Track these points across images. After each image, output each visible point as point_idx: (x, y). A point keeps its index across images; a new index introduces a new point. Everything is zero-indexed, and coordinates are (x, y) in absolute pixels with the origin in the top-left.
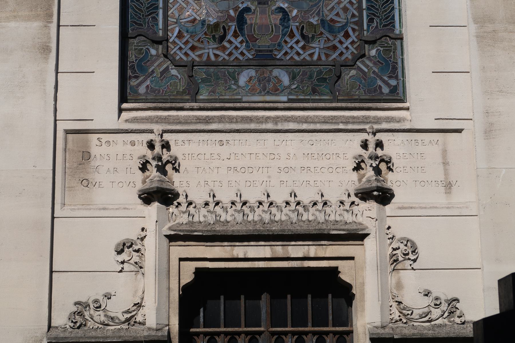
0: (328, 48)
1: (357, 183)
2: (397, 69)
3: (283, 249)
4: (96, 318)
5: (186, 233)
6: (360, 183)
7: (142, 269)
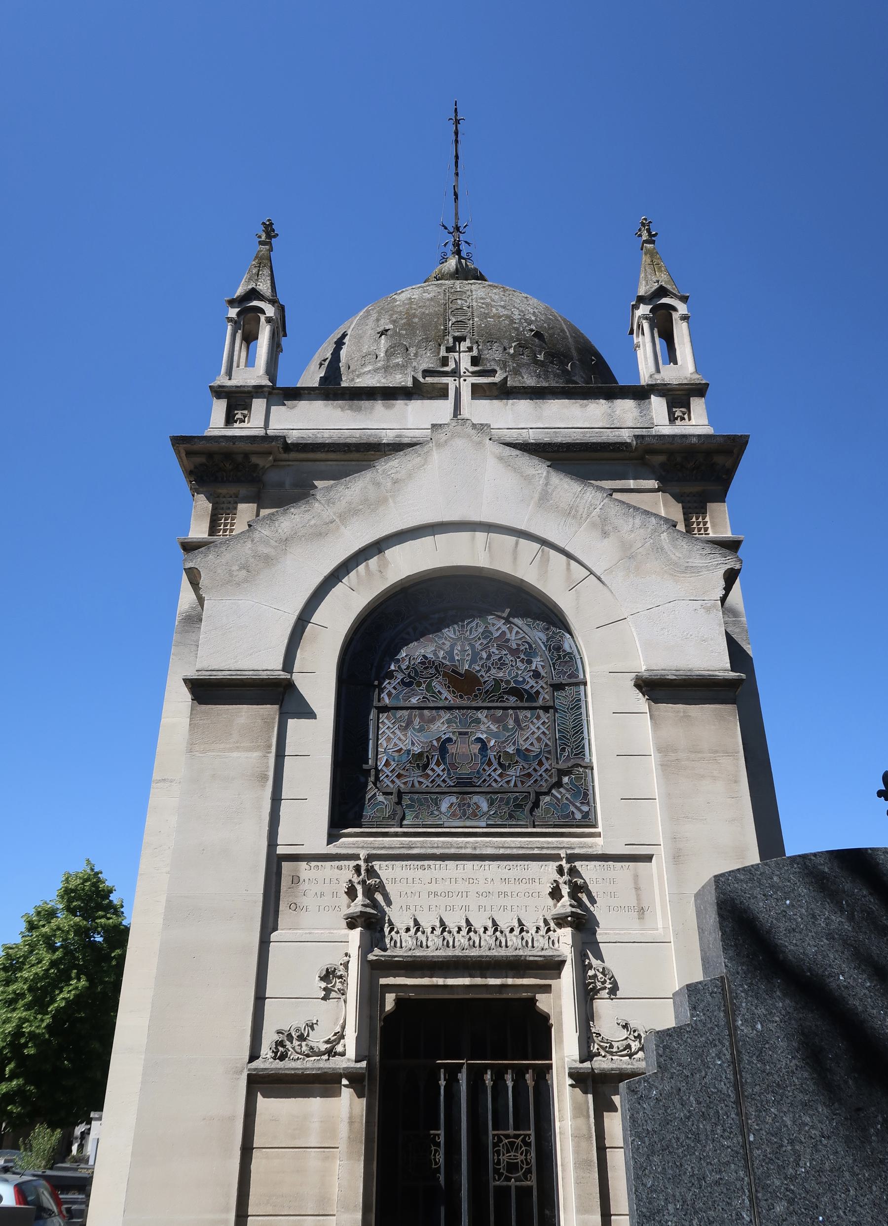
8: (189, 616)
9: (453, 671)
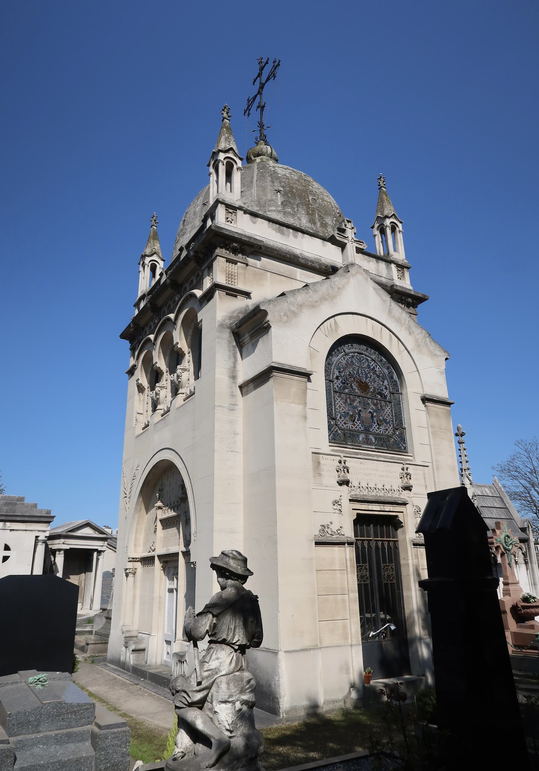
8: (222, 324)
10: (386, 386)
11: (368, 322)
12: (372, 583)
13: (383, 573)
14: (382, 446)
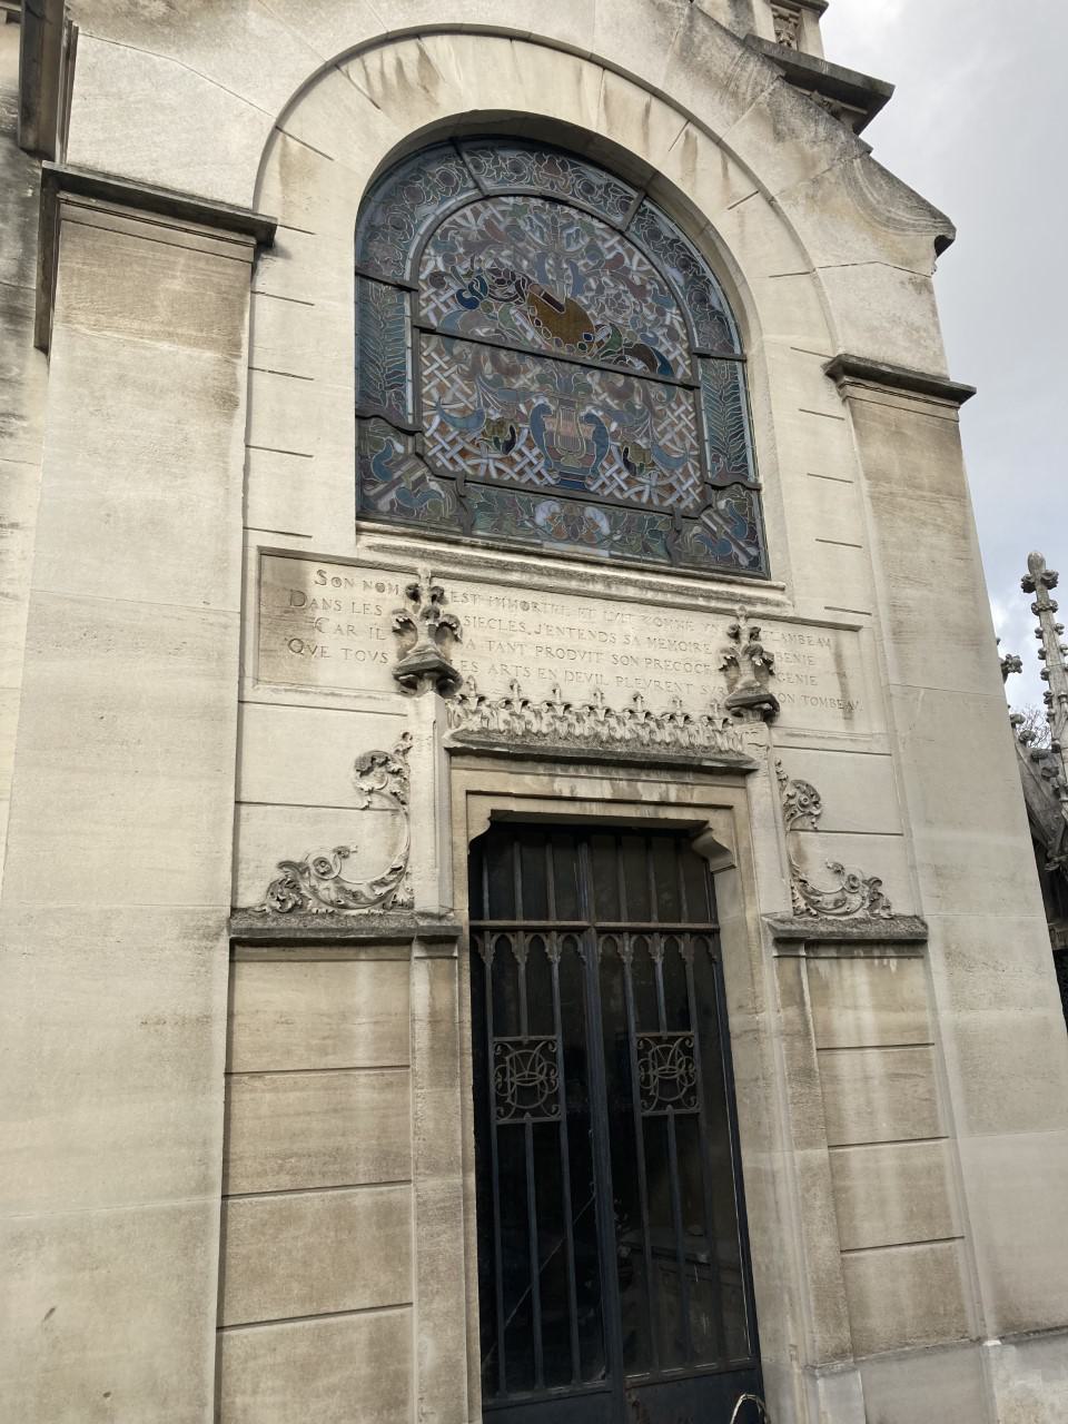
0: (663, 486)
1: (726, 692)
2: (756, 532)
3: (628, 786)
4: (323, 894)
5: (481, 748)
6: (731, 691)
7: (405, 807)
9: (547, 297)
10: (671, 329)
11: (585, 72)
12: (579, 1122)
13: (637, 1074)
14: (646, 549)
